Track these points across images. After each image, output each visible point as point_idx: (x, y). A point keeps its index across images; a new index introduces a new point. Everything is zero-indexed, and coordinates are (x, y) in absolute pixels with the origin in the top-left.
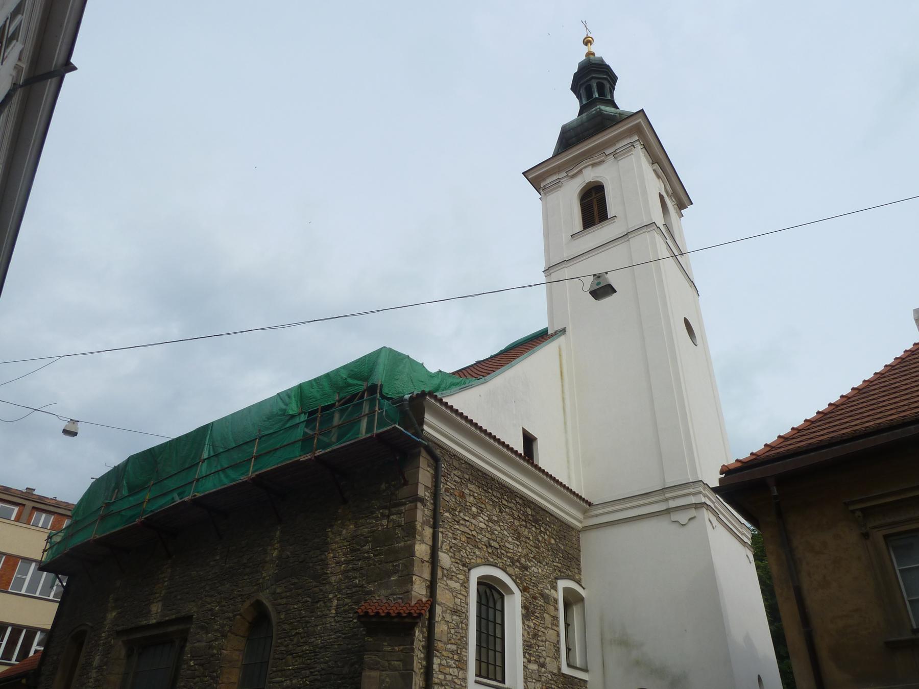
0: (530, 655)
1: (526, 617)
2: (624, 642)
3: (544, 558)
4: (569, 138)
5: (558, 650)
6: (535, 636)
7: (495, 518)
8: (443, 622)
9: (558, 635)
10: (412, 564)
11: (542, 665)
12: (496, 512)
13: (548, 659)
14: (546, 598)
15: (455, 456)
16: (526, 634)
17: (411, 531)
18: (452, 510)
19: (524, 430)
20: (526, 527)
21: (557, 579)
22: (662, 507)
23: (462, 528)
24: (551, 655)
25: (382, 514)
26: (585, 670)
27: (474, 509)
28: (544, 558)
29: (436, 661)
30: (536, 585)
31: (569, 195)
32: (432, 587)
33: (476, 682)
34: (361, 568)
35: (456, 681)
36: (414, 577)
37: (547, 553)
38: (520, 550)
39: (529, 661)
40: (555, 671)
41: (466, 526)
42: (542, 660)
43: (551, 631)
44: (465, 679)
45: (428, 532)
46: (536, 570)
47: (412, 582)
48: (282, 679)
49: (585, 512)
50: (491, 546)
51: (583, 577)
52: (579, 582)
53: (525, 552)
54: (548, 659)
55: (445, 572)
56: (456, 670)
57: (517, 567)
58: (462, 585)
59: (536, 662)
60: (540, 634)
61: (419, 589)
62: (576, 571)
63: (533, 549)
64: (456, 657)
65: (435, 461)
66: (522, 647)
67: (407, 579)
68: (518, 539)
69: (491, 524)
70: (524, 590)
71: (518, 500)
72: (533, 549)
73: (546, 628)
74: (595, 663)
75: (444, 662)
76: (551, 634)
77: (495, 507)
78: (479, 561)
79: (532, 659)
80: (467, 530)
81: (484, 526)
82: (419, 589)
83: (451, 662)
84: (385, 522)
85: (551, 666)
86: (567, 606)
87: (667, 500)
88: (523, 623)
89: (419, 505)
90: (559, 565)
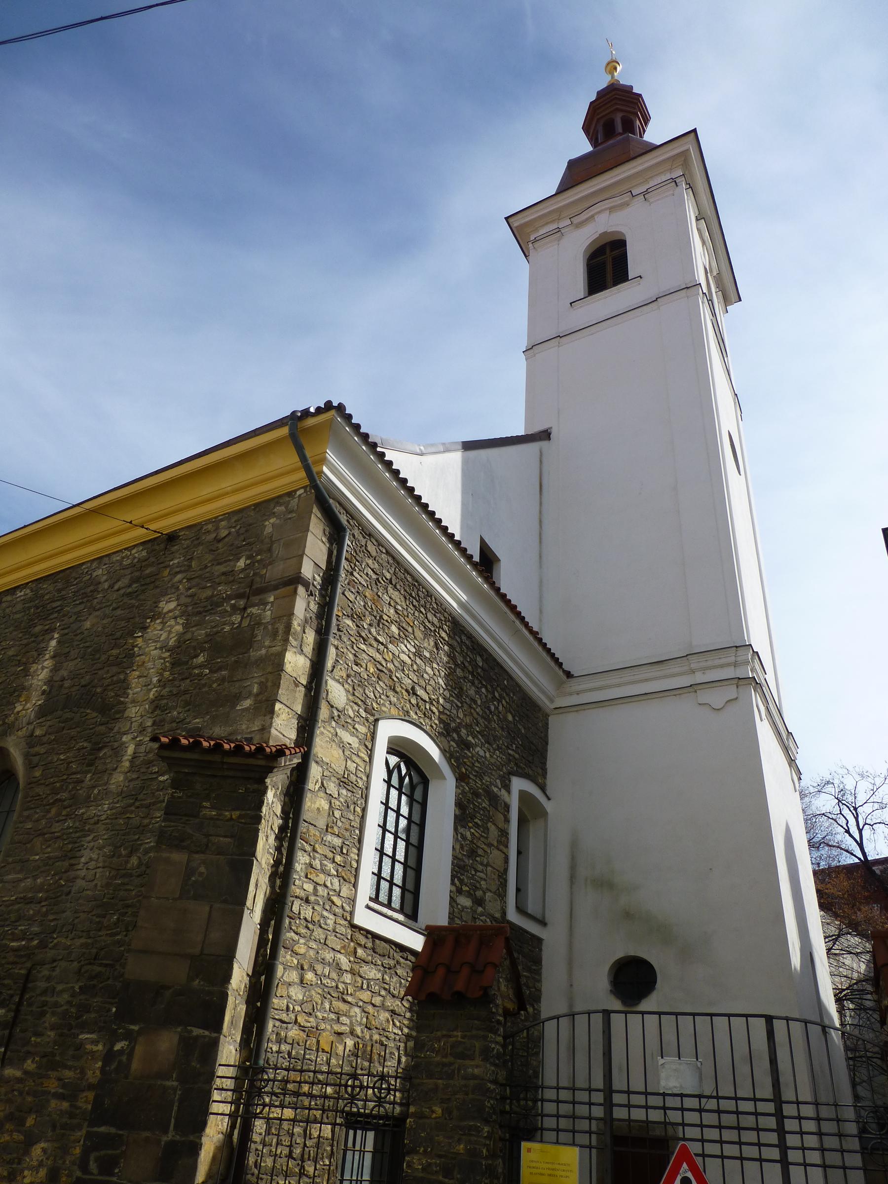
0: (461, 881)
1: (463, 817)
2: (604, 884)
3: (496, 738)
4: (577, 172)
5: (504, 884)
6: (472, 853)
7: (427, 655)
8: (322, 794)
9: (506, 860)
10: (277, 686)
11: (479, 902)
12: (429, 644)
13: (488, 894)
14: (494, 800)
15: (369, 534)
16: (458, 847)
17: (283, 630)
18: (356, 617)
19: (481, 538)
20: (473, 683)
21: (511, 773)
22: (685, 681)
23: (372, 652)
24: (494, 888)
25: (234, 607)
26: (543, 923)
27: (394, 629)
28: (496, 738)
29: (301, 860)
30: (479, 775)
31: (570, 254)
32: (307, 725)
33: (368, 907)
34: (186, 692)
35: (335, 899)
36: (278, 706)
37: (499, 733)
38: (461, 715)
39: (459, 891)
40: (498, 915)
41: (378, 650)
42: (479, 893)
43: (496, 852)
44: (353, 901)
45: (310, 637)
46: (482, 753)
47: (272, 712)
48: (20, 876)
49: (559, 685)
50: (415, 694)
51: (551, 781)
52: (543, 788)
53: (468, 720)
54: (488, 894)
55: (336, 713)
56: (336, 881)
57: (454, 740)
58: (362, 743)
59: (469, 895)
60: (480, 852)
61: (284, 728)
62: (540, 771)
63: (481, 721)
64: (338, 859)
65: (336, 534)
66: (449, 867)
67: (266, 707)
68: (459, 697)
69: (418, 661)
70: (461, 778)
71: (464, 638)
72: (481, 721)
73: (490, 845)
74: (557, 914)
75: (317, 863)
76: (495, 856)
77: (426, 636)
78: (394, 711)
79: (465, 888)
80: (378, 657)
81: (409, 661)
82: (284, 728)
83: (330, 866)
84: (236, 619)
85: (493, 907)
86: (523, 821)
87: (693, 672)
88: (456, 829)
89: (301, 590)
90: (517, 756)
